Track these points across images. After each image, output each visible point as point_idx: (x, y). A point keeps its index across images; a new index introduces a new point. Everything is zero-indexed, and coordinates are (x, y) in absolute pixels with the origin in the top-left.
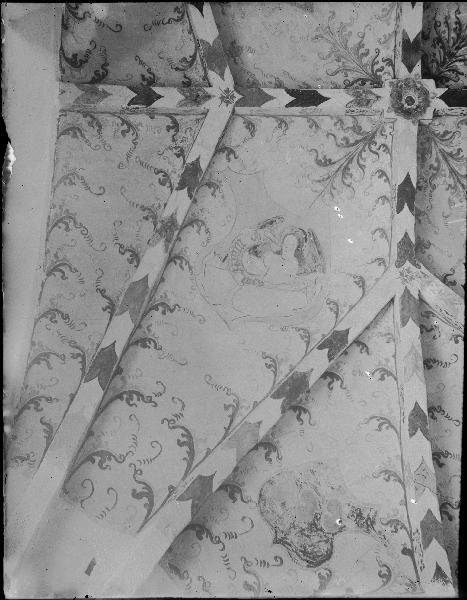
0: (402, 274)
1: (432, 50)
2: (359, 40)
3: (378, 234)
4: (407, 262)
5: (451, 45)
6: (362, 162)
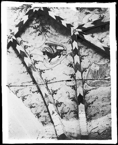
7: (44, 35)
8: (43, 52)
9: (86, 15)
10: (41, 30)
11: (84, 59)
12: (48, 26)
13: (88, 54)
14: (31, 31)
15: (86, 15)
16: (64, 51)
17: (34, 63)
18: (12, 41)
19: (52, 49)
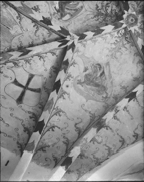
2: (113, 44)
5: (103, 16)
9: (85, 67)
11: (34, 26)
15: (85, 67)
16: (59, 17)
19: (71, 10)
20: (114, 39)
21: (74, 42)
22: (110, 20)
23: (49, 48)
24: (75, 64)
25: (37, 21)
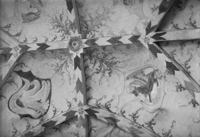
0: (17, 47)
1: (101, 53)
2: (103, 24)
3: (35, 39)
4: (21, 49)
5: (106, 60)
6: (61, 31)
7: (115, 70)
8: (134, 92)
9: (142, 3)
10: (107, 68)
11: (189, 67)
12: (111, 56)
13: (190, 55)
14: (98, 79)
15: (142, 3)
16: (157, 73)
17: (133, 120)
18: (86, 113)
19: (140, 79)
20: (100, 30)
21: (146, 35)
22: (100, 54)
23: (178, 33)
24: (152, 9)
25: (183, 71)
